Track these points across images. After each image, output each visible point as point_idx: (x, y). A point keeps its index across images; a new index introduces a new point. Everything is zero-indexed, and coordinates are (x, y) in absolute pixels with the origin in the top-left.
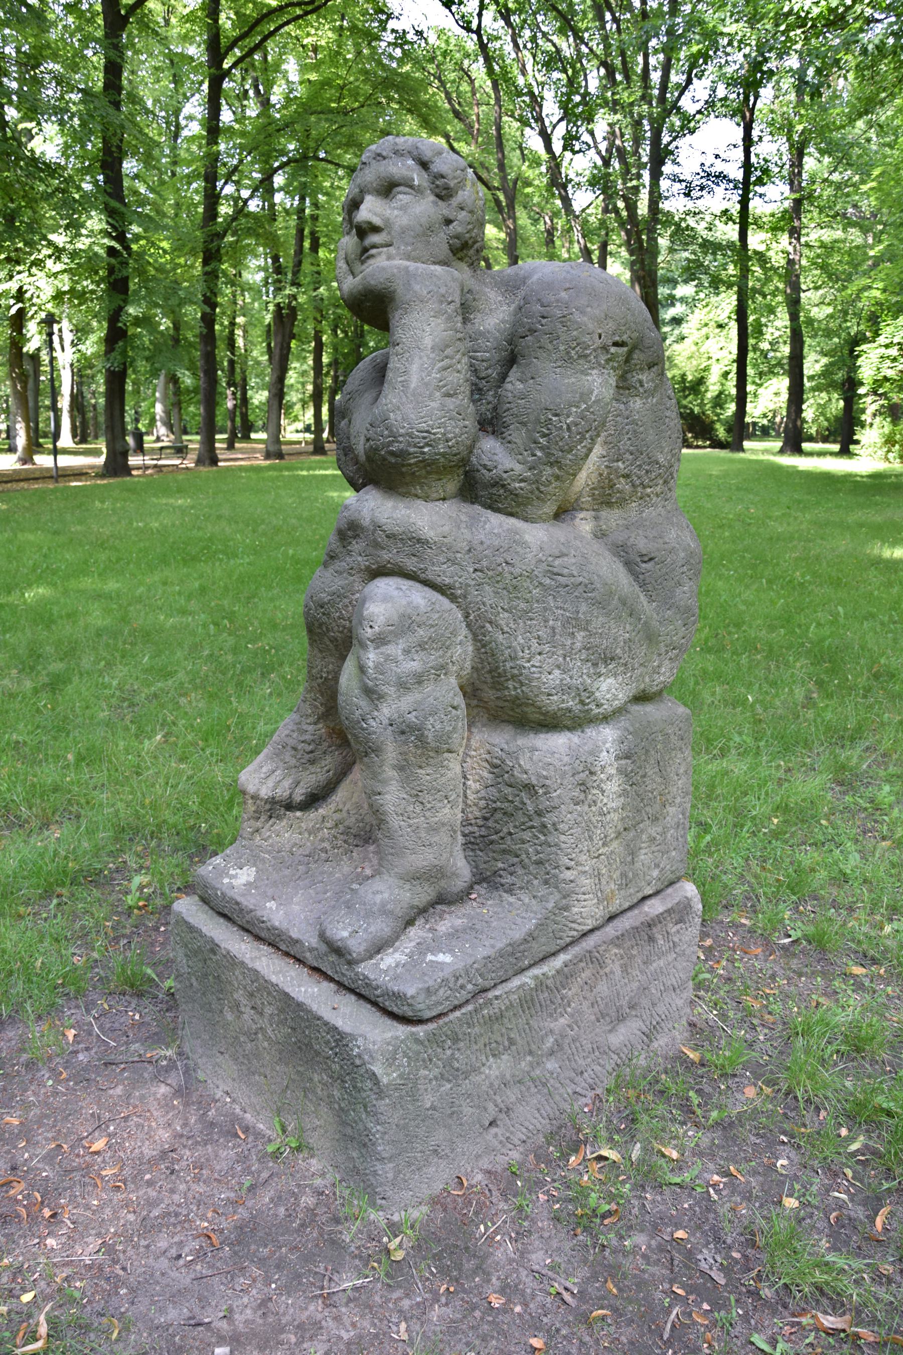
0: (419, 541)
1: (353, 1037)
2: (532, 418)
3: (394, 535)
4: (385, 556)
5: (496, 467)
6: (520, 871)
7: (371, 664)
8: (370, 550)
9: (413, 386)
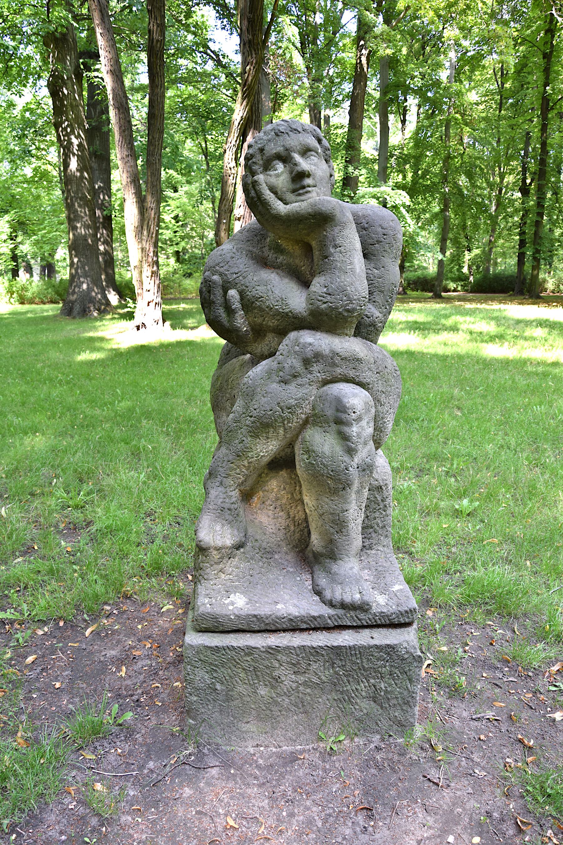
0: (358, 360)
1: (401, 644)
2: (386, 288)
3: (346, 358)
4: (339, 370)
5: (372, 316)
6: (374, 535)
7: (355, 434)
8: (329, 368)
9: (358, 271)
